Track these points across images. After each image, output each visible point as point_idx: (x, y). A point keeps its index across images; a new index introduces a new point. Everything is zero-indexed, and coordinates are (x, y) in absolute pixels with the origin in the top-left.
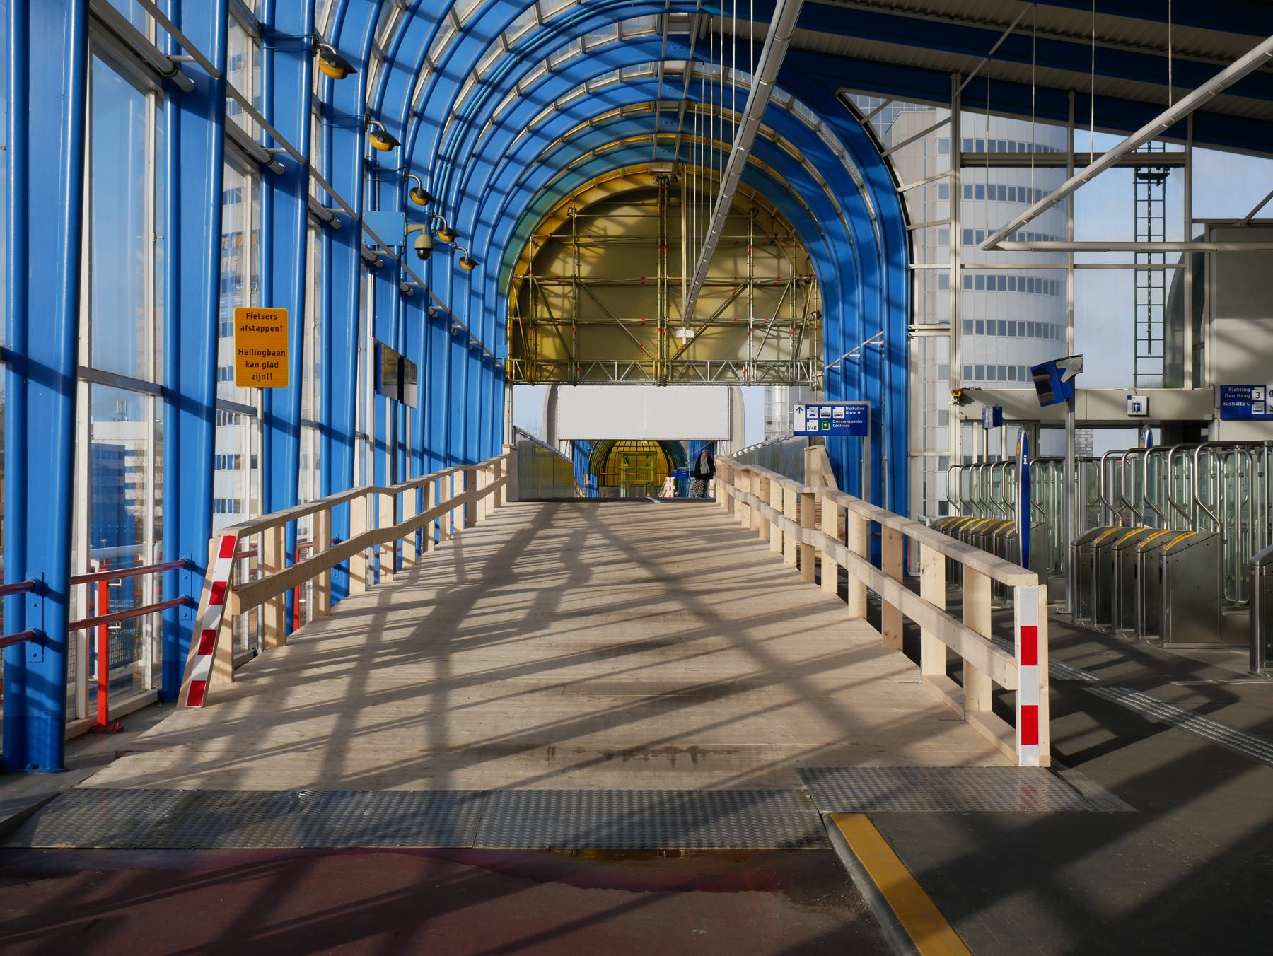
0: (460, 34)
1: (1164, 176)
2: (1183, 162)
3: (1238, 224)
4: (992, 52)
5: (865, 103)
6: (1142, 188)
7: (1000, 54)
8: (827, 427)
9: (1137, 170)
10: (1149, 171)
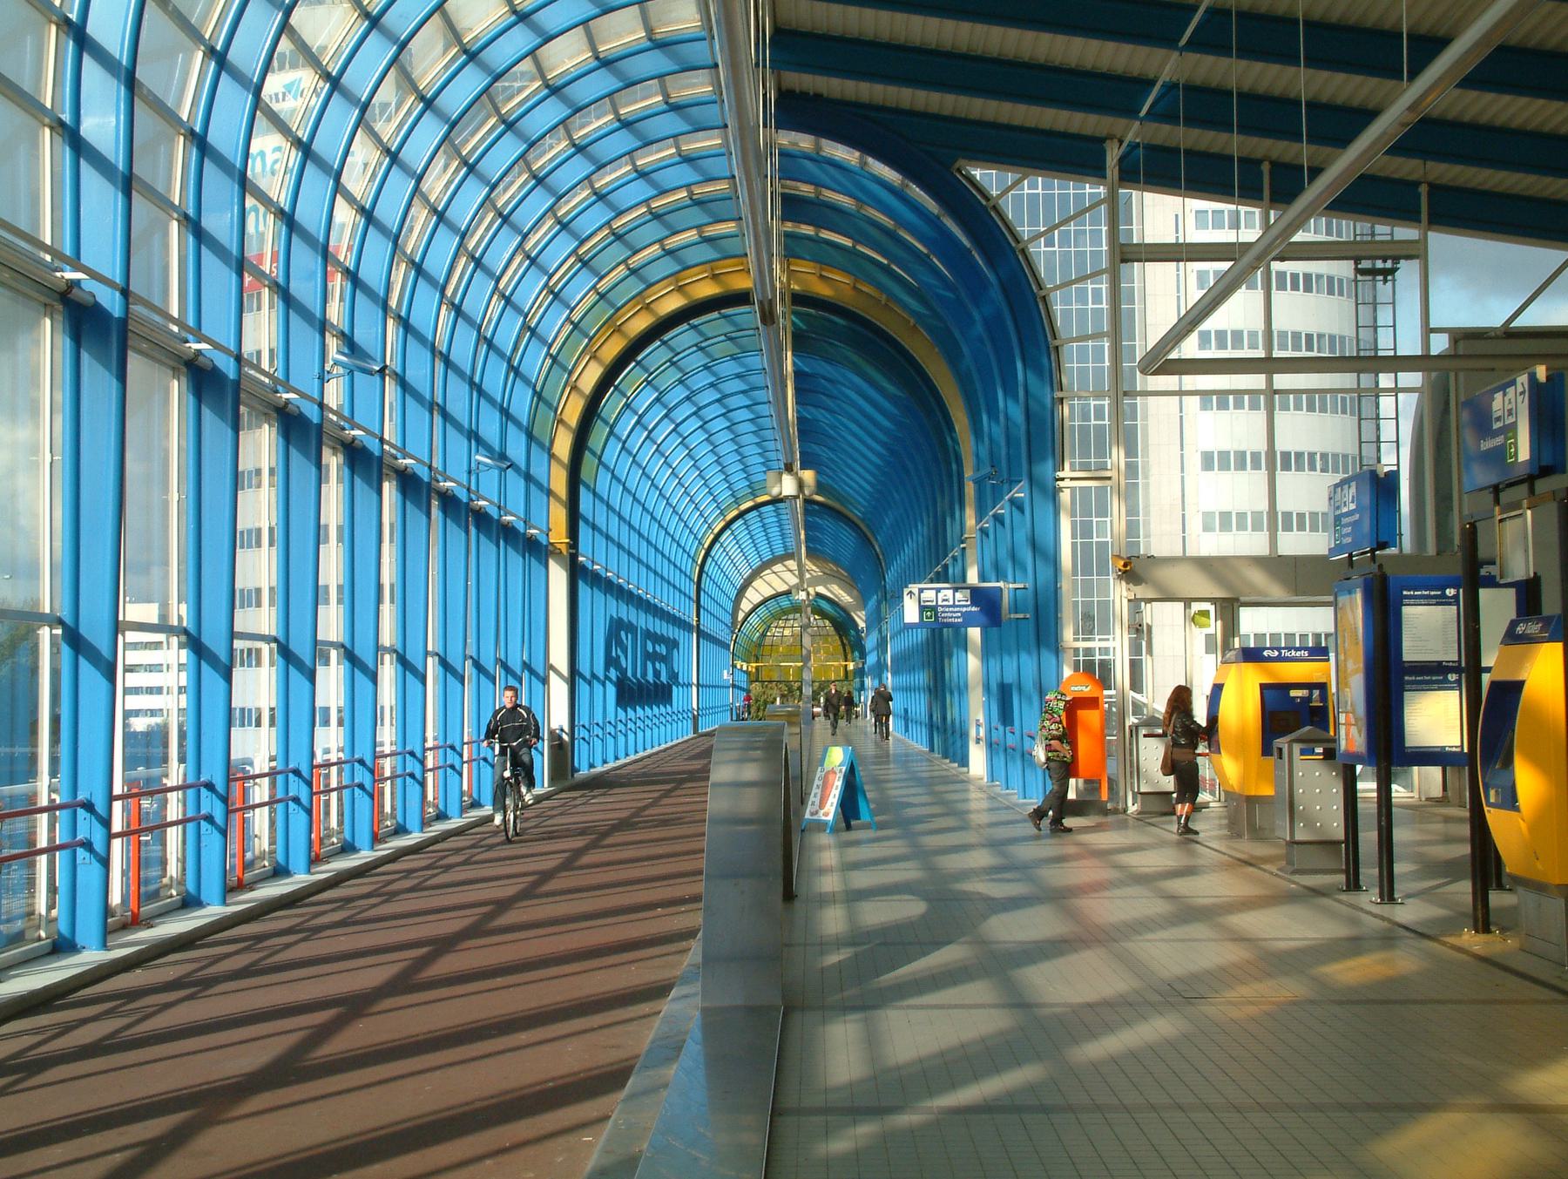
0: (513, 18)
1: (1393, 271)
2: (1416, 252)
5: (984, 175)
9: (1356, 264)
10: (1374, 264)
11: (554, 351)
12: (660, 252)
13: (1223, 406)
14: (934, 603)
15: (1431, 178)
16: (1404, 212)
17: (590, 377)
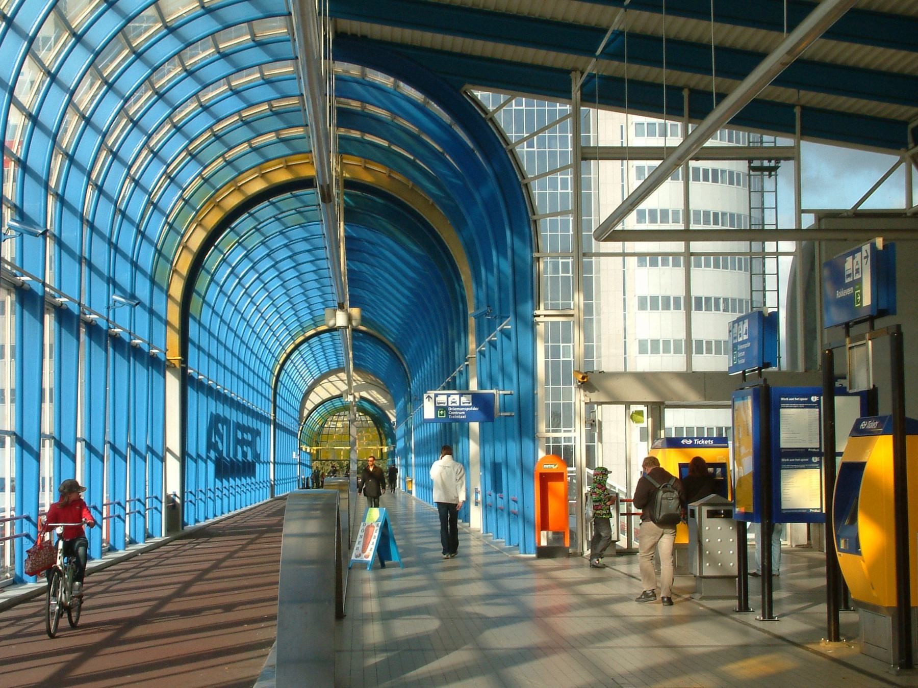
1: (775, 169)
3: (846, 214)
4: (598, 53)
6: (755, 180)
7: (608, 55)
9: (750, 163)
10: (762, 163)
11: (170, 220)
12: (248, 149)
13: (654, 264)
14: (446, 405)
15: (803, 102)
16: (785, 128)
17: (197, 239)
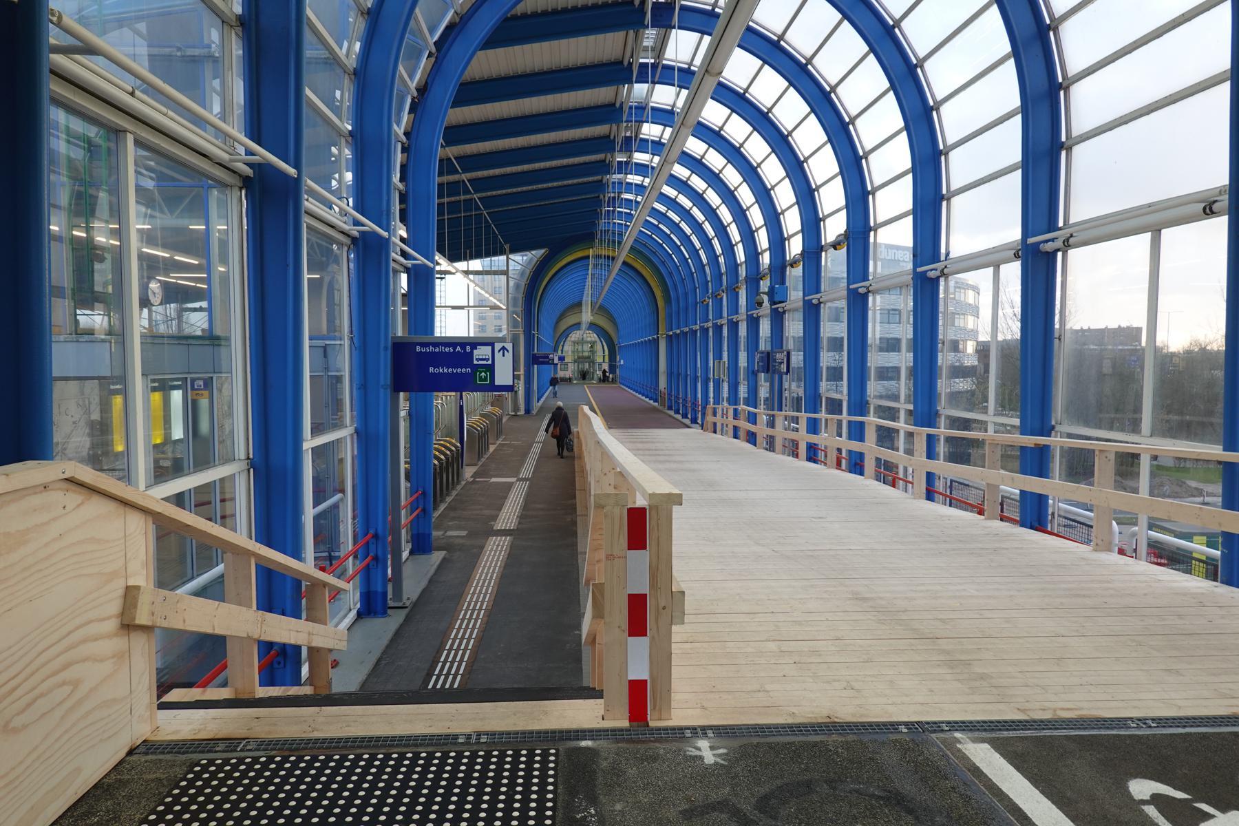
8: (485, 379)
